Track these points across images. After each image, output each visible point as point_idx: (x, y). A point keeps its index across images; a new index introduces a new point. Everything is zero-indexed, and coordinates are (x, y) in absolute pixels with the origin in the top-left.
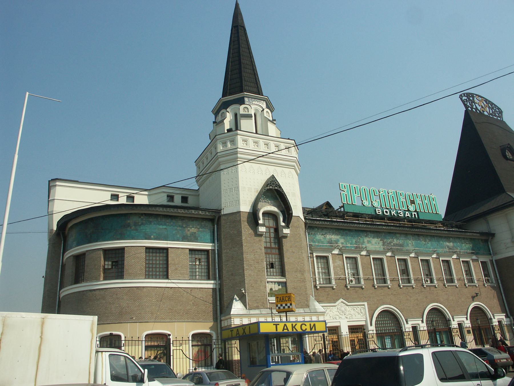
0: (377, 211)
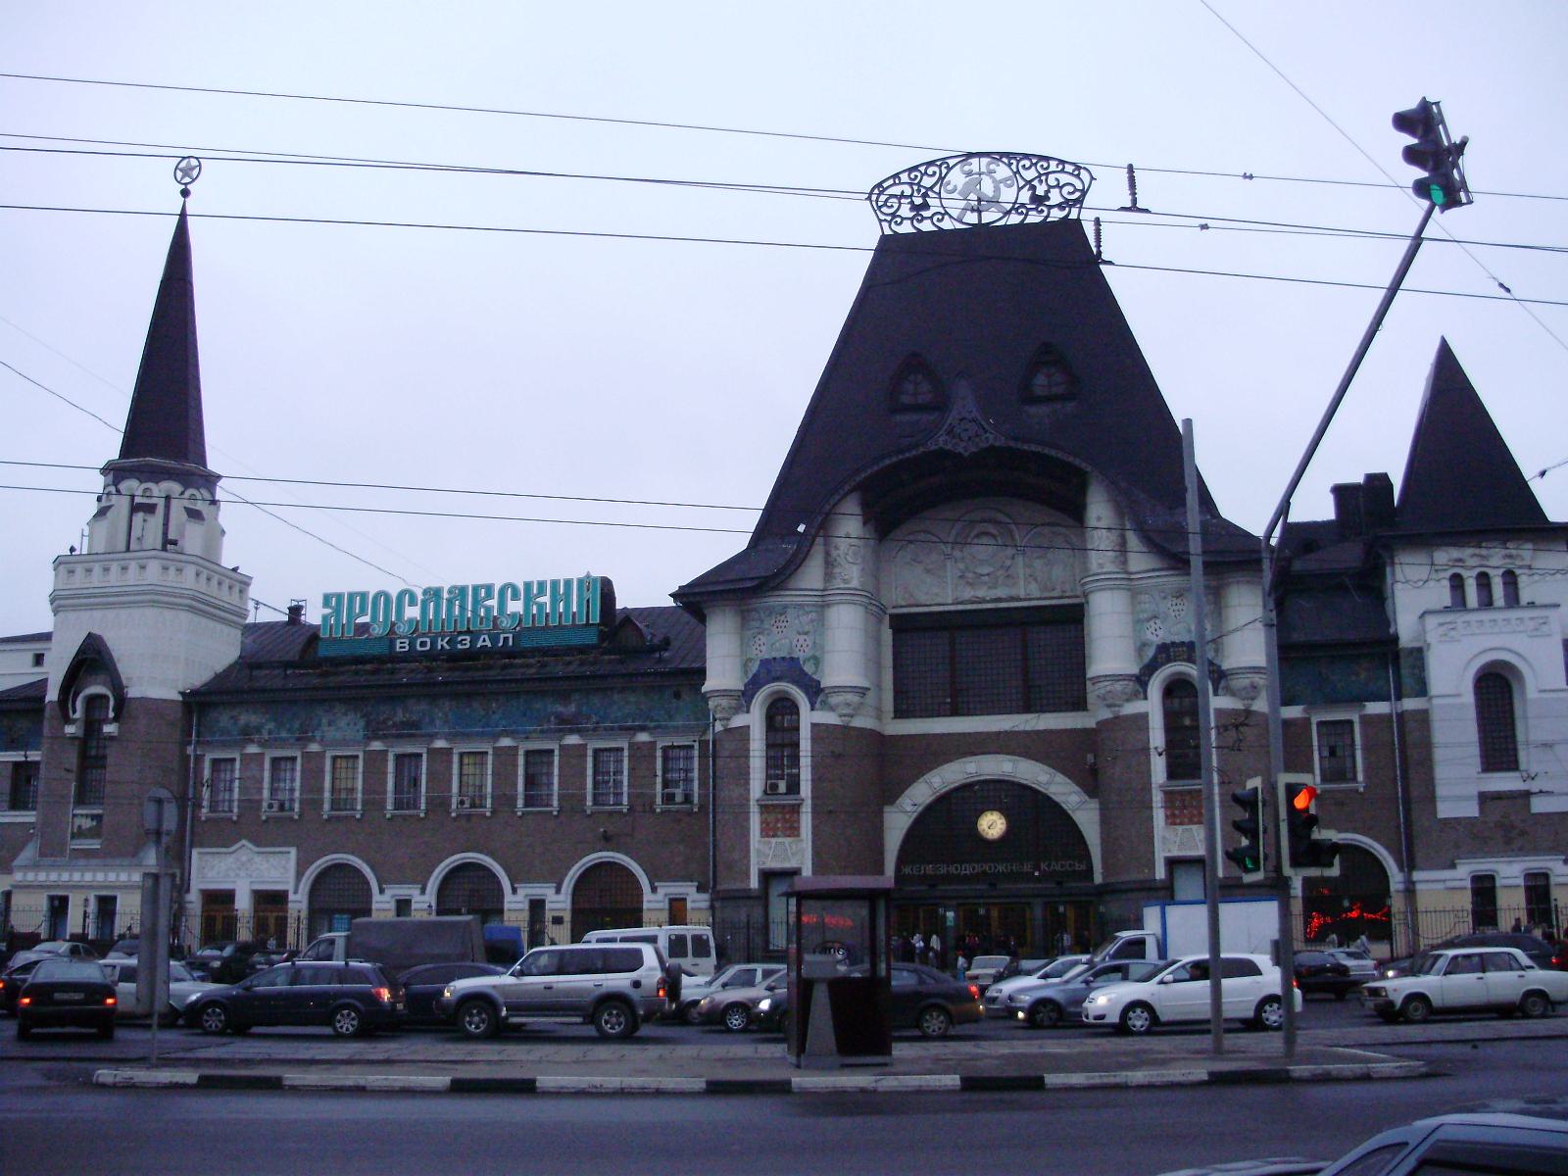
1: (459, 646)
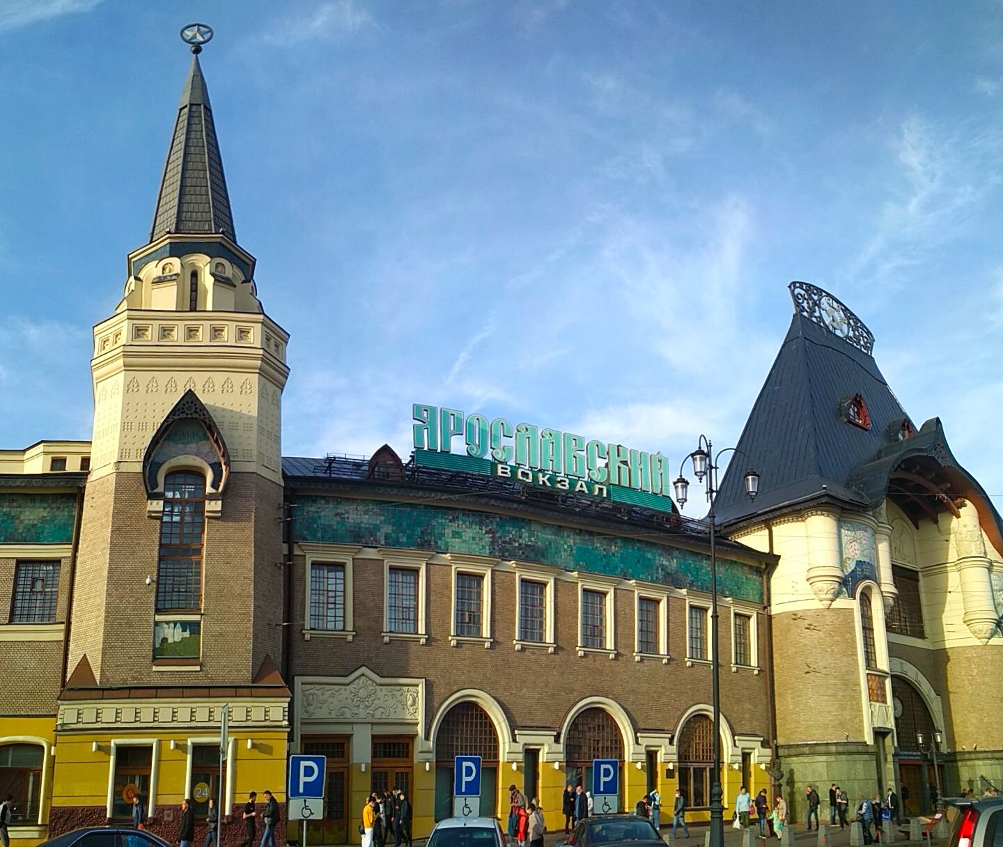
0: (500, 470)
1: (559, 486)
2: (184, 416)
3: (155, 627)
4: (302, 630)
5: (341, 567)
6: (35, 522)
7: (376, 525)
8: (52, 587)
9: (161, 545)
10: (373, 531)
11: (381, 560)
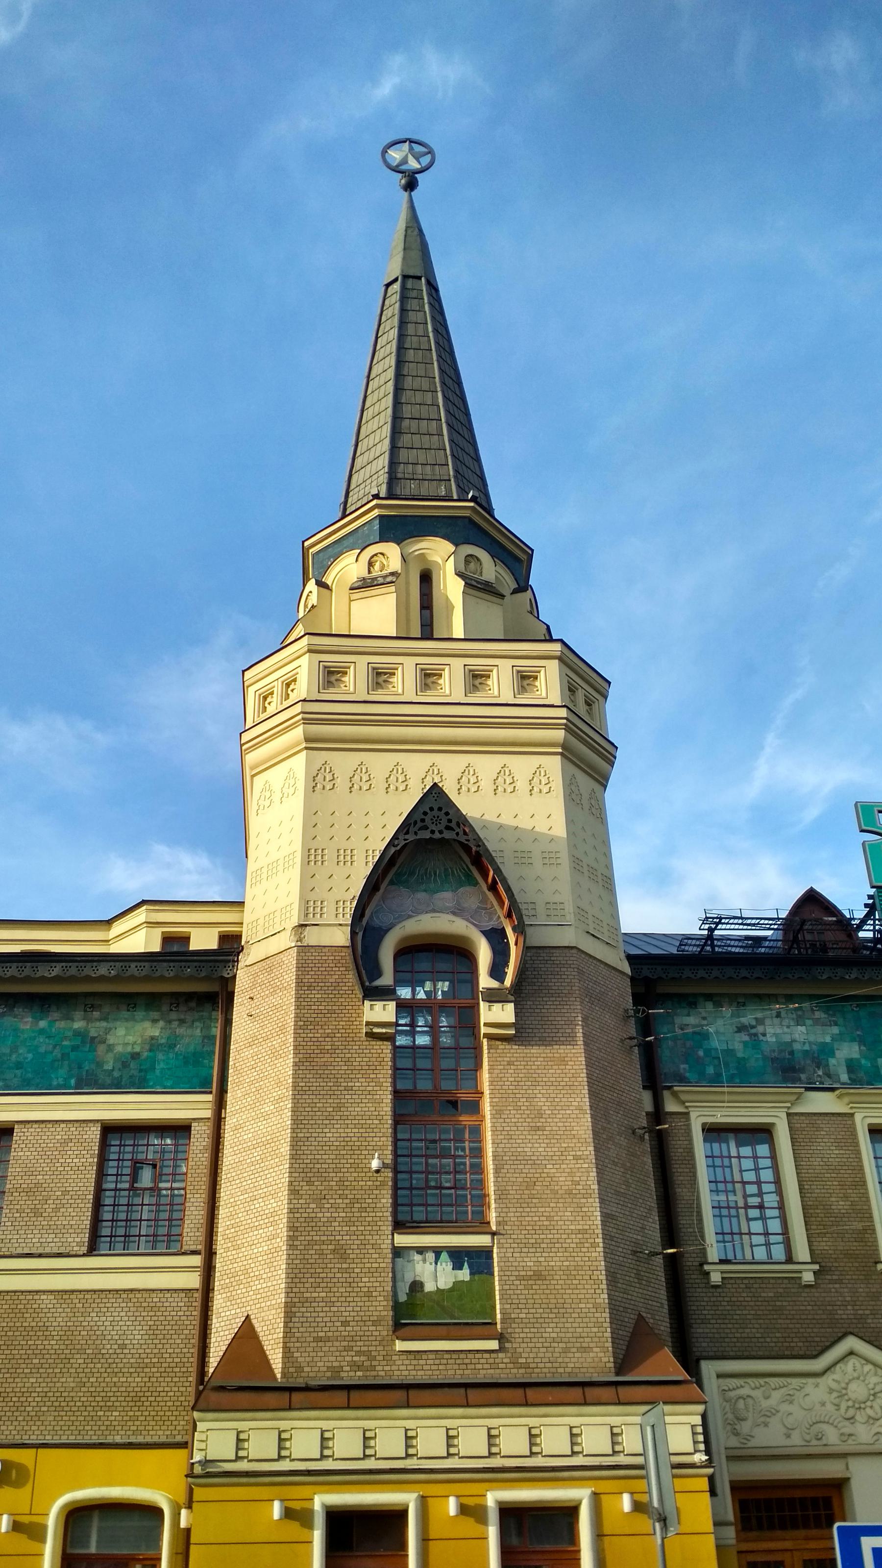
2: (426, 835)
3: (393, 1258)
4: (701, 1265)
5: (762, 1133)
6: (137, 1049)
7: (825, 1044)
8: (174, 1181)
9: (396, 1093)
10: (820, 1056)
11: (845, 1114)
